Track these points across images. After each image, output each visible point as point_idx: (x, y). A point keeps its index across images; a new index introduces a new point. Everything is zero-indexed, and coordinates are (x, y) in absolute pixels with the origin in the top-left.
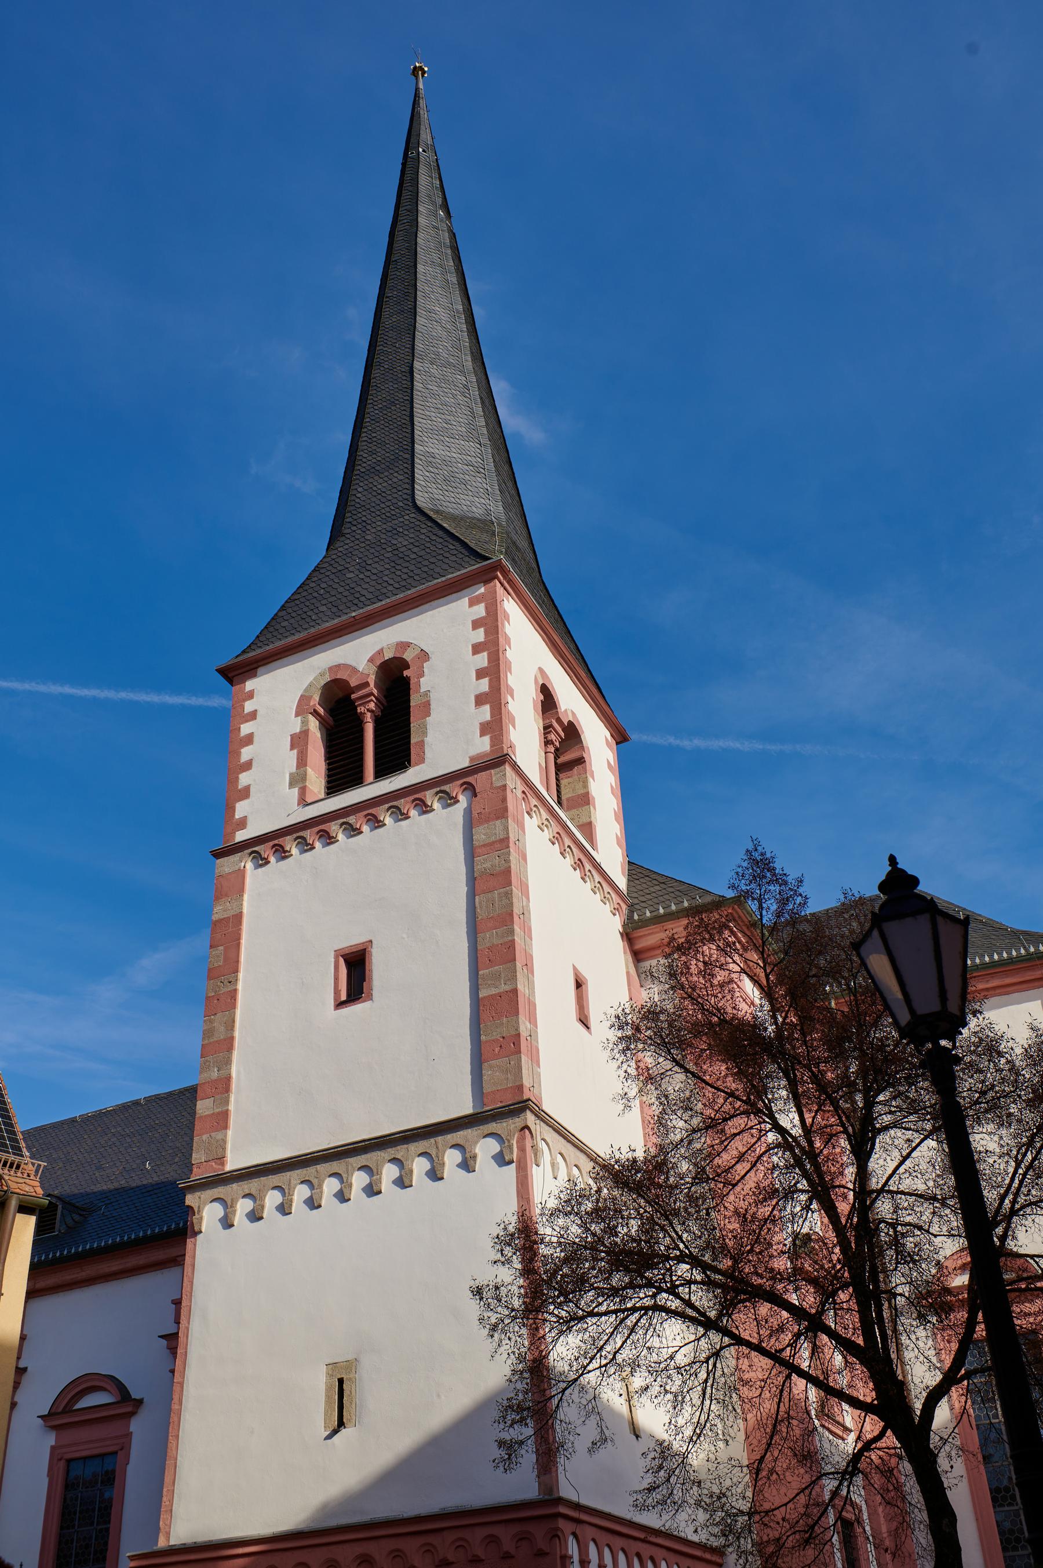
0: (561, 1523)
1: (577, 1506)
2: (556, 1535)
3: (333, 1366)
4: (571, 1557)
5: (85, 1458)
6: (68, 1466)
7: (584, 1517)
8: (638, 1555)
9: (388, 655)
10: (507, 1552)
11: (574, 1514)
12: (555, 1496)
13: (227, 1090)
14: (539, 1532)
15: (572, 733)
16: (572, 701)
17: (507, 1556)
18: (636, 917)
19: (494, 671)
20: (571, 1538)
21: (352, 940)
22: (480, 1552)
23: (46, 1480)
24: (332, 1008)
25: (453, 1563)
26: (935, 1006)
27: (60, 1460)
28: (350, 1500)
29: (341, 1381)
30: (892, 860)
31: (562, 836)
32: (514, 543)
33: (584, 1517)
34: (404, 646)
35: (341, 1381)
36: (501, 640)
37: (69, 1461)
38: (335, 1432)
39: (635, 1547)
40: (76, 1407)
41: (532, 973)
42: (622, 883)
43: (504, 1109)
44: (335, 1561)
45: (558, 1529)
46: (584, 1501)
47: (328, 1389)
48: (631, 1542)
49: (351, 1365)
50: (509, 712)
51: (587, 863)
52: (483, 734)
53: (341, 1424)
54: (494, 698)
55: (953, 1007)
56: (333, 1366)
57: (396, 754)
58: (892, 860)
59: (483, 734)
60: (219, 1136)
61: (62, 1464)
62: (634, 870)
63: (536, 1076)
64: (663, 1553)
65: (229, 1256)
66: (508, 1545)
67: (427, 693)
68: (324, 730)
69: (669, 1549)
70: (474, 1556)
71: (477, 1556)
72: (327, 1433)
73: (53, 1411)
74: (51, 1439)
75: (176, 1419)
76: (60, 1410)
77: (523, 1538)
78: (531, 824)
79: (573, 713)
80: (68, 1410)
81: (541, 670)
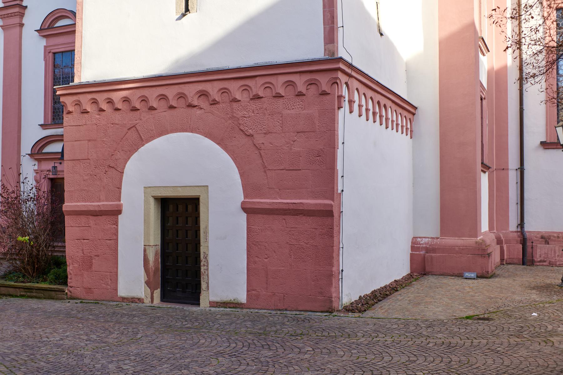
2: (335, 82)
4: (345, 98)
5: (62, 52)
6: (54, 56)
7: (354, 74)
10: (300, 92)
11: (349, 71)
12: (336, 56)
14: (324, 80)
17: (300, 94)
20: (345, 86)
22: (282, 92)
23: (44, 62)
25: (262, 97)
27: (50, 52)
28: (193, 58)
37: (54, 53)
38: (184, 15)
40: (56, 25)
44: (184, 94)
45: (337, 78)
46: (354, 64)
48: (376, 94)
53: (187, 10)
61: (51, 54)
66: (301, 87)
69: (393, 102)
70: (277, 93)
71: (279, 93)
72: (178, 16)
73: (42, 28)
74: (44, 42)
75: (80, 8)
76: (46, 27)
77: (311, 83)
80: (50, 27)
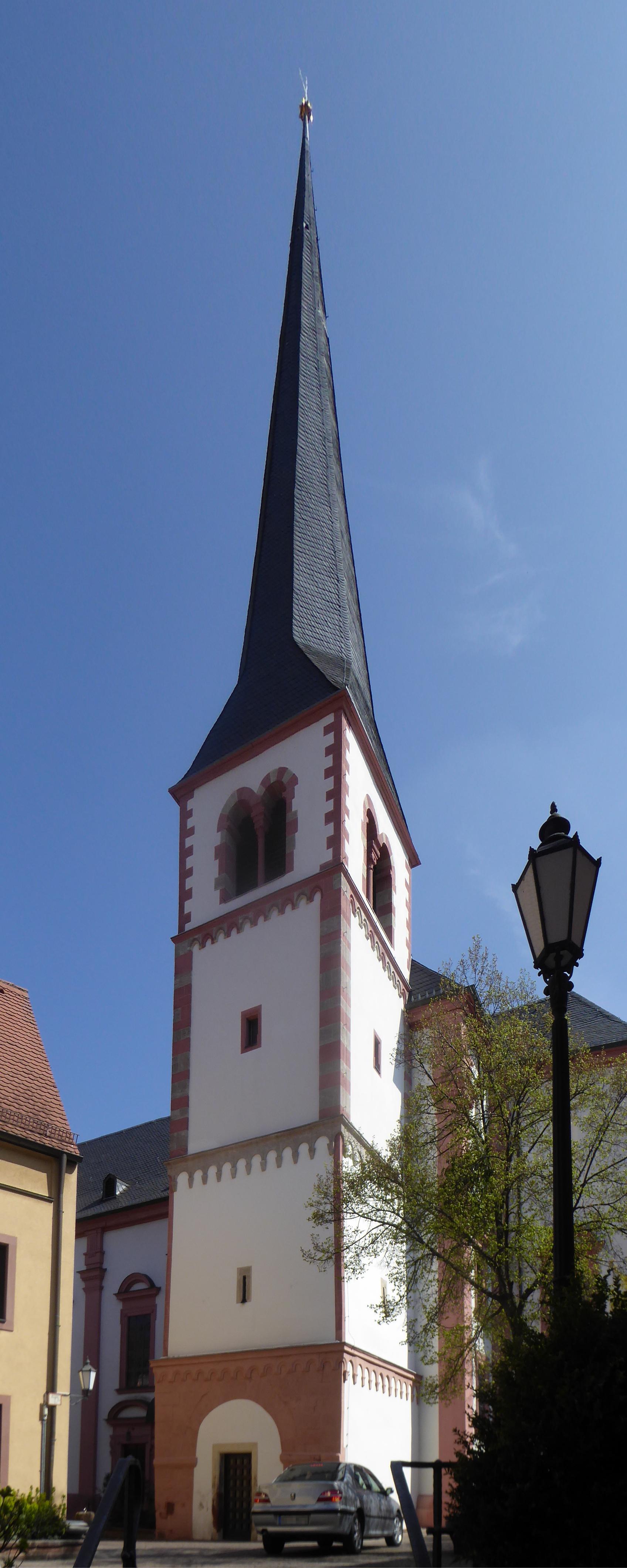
0: (345, 1355)
1: (353, 1348)
3: (240, 1270)
7: (356, 1353)
8: (381, 1375)
9: (273, 779)
13: (187, 1105)
15: (385, 852)
16: (386, 828)
18: (413, 999)
19: (336, 794)
21: (244, 1265)
24: (240, 1050)
26: (563, 937)
29: (244, 1278)
30: (554, 808)
31: (373, 934)
32: (357, 681)
33: (356, 1353)
34: (282, 771)
35: (244, 1278)
36: (343, 766)
39: (380, 1370)
41: (350, 1030)
42: (407, 974)
43: (330, 1122)
47: (238, 1281)
49: (248, 1269)
50: (346, 807)
51: (387, 957)
52: (327, 755)
54: (335, 817)
55: (575, 940)
56: (240, 1270)
57: (278, 860)
58: (554, 808)
59: (327, 755)
60: (183, 1133)
62: (415, 966)
63: (348, 1100)
64: (393, 1374)
65: (190, 1199)
67: (296, 812)
68: (236, 799)
69: (396, 1373)
78: (355, 921)
79: (387, 838)
81: (368, 796)
